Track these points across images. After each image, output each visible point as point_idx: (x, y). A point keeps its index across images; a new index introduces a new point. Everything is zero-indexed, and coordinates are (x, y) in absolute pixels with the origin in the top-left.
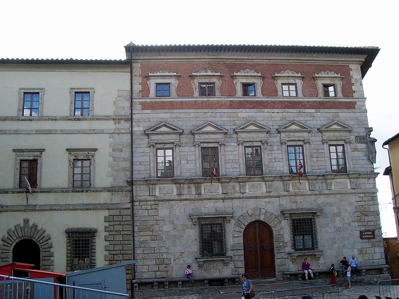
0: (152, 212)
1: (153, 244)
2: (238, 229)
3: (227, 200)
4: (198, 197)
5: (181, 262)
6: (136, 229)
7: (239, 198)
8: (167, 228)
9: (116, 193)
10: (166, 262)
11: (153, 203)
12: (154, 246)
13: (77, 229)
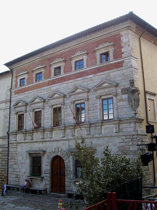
0: (15, 149)
6: (9, 158)
7: (49, 141)
9: (4, 140)
12: (15, 167)
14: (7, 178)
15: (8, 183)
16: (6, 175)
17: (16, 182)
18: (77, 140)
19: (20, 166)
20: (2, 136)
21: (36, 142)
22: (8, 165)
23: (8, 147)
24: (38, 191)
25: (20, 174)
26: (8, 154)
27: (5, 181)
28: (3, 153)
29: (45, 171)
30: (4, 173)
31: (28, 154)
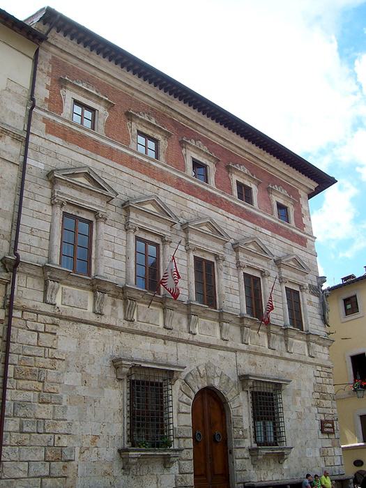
1: (43, 412)
4: (129, 325)
11: (49, 320)
12: (44, 415)
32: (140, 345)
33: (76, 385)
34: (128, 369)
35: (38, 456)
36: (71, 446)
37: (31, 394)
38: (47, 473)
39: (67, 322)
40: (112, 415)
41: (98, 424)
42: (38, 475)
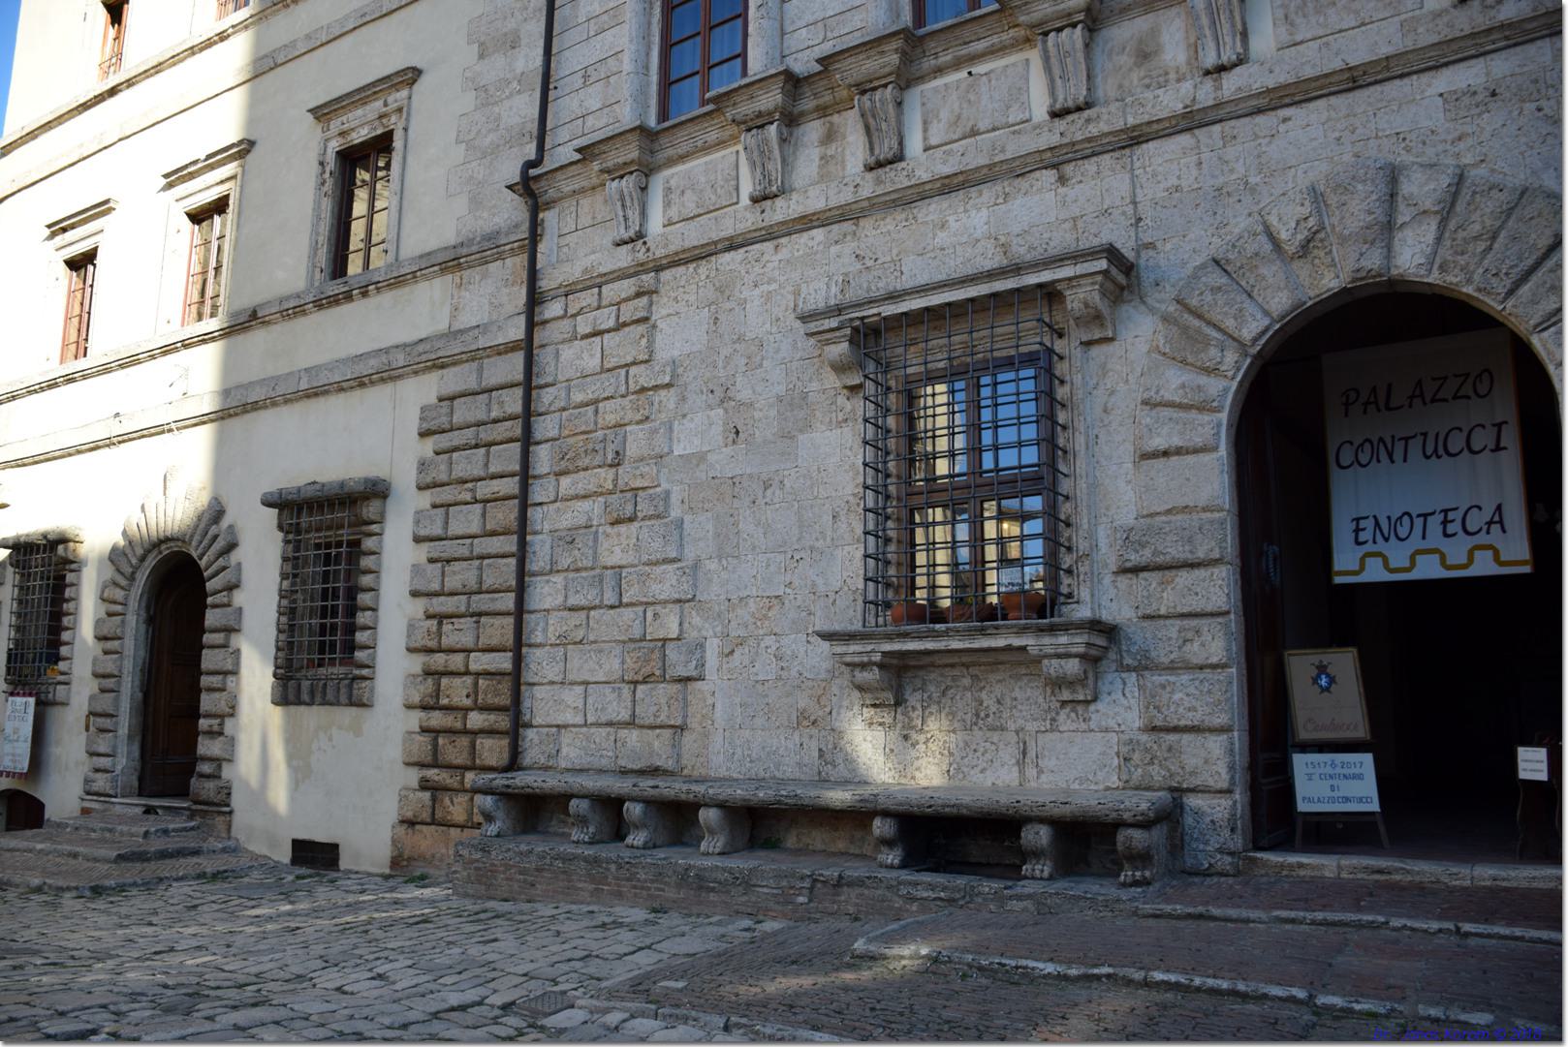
0: (623, 346)
1: (617, 548)
2: (1174, 381)
3: (1090, 166)
4: (879, 182)
5: (766, 669)
6: (543, 458)
7: (1191, 121)
8: (703, 894)
9: (475, 274)
10: (679, 662)
11: (627, 287)
12: (617, 558)
13: (342, 484)
14: (505, 700)
15: (527, 759)
16: (504, 662)
17: (632, 737)
18: (324, 964)
19: (701, 529)
20: (453, 242)
21: (951, 186)
22: (523, 544)
23: (528, 346)
24: (1038, 836)
25: (692, 635)
26: (528, 415)
27: (490, 732)
28: (464, 412)
29: (1129, 538)
30: (467, 639)
31: (840, 349)
32: (942, 235)
33: (704, 449)
34: (845, 345)
35: (607, 667)
36: (695, 634)
37: (584, 506)
38: (624, 715)
39: (681, 269)
40: (827, 518)
41: (780, 558)
42: (603, 719)
